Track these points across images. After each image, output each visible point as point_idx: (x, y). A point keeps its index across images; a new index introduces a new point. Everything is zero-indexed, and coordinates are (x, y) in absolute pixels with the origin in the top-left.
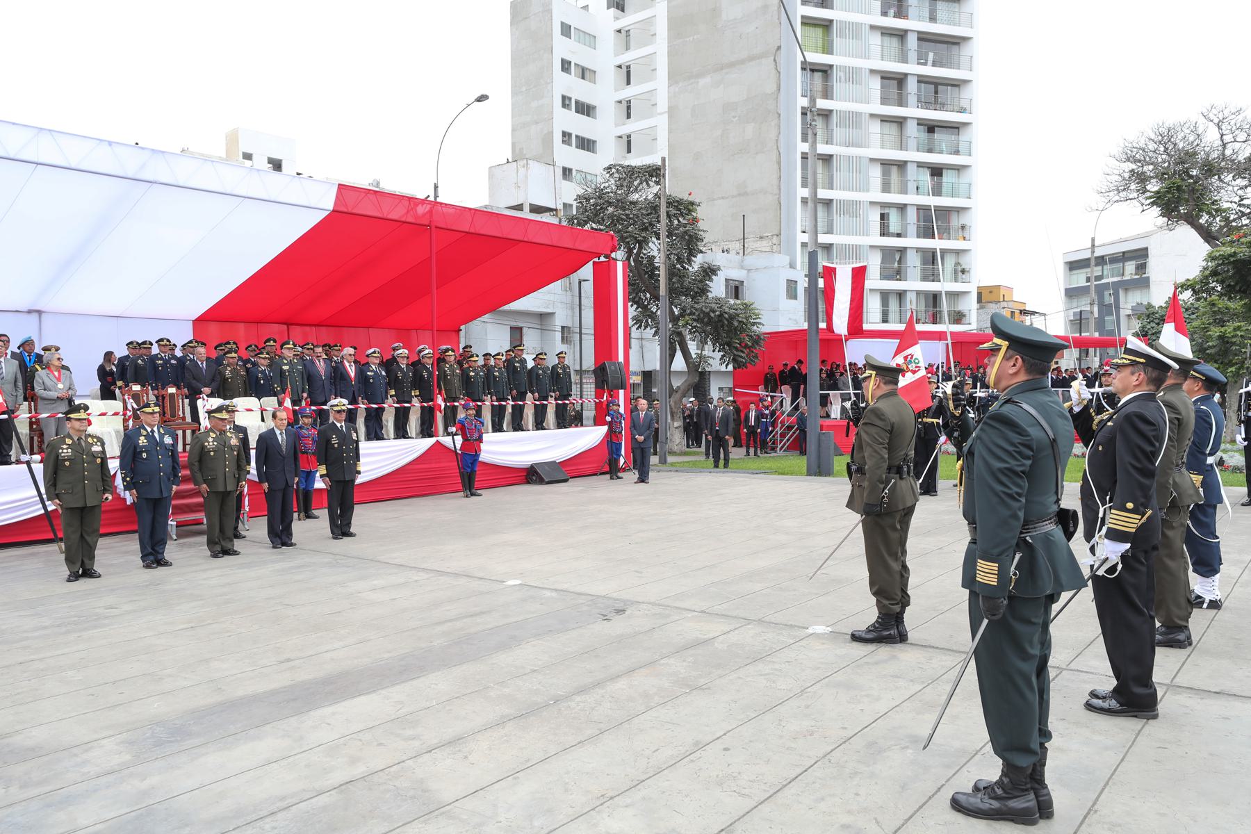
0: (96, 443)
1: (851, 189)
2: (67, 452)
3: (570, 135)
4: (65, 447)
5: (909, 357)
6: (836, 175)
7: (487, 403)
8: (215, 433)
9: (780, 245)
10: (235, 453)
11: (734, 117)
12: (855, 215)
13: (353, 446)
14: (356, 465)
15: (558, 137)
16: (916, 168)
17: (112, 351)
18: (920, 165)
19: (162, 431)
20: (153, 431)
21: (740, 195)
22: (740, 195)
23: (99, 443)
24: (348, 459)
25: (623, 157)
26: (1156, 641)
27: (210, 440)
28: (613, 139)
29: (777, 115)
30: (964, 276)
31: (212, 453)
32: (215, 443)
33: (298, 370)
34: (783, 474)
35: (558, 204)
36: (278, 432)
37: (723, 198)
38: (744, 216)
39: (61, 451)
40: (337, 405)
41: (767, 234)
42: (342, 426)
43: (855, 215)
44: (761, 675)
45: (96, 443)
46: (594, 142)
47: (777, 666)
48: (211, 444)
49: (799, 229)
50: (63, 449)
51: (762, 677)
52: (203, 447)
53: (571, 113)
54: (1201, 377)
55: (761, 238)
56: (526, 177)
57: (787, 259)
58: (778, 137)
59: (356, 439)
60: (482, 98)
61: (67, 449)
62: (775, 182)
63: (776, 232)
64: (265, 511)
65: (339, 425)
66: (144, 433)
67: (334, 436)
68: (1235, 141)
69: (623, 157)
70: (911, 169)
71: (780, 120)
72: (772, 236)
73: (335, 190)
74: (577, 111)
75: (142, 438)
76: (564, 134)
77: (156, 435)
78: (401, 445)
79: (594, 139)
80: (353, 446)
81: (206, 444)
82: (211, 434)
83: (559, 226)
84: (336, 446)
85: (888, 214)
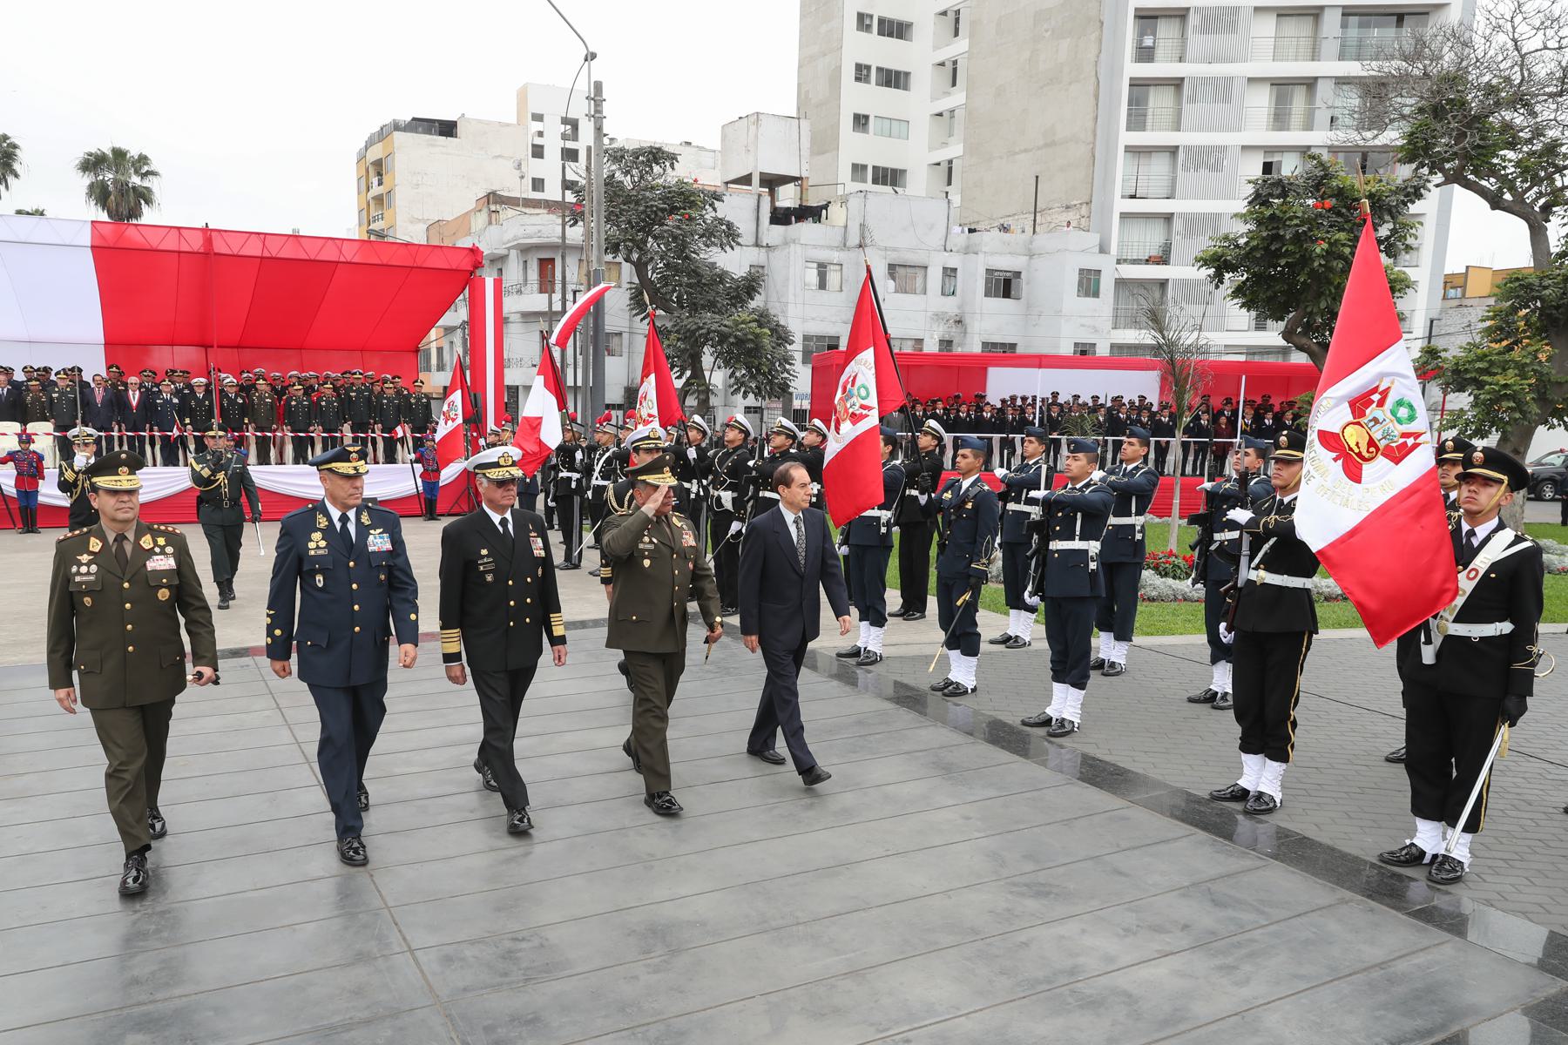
0: (162, 548)
1: (1211, 129)
2: (88, 573)
3: (868, 68)
4: (85, 558)
5: (1376, 397)
6: (1187, 108)
9: (1089, 217)
11: (1047, 31)
12: (1216, 167)
13: (534, 577)
15: (849, 72)
16: (1333, 86)
18: (1341, 81)
19: (365, 519)
20: (344, 519)
21: (1046, 145)
22: (1046, 145)
23: (169, 550)
25: (944, 93)
28: (930, 67)
29: (1099, 24)
30: (1407, 257)
34: (901, 657)
35: (803, 169)
37: (1026, 151)
38: (1037, 177)
39: (74, 569)
40: (496, 465)
41: (1075, 202)
42: (504, 522)
43: (1216, 167)
45: (162, 548)
46: (907, 74)
49: (1118, 193)
50: (80, 564)
53: (874, 37)
55: (1068, 207)
56: (756, 136)
57: (1093, 239)
58: (1098, 57)
59: (543, 553)
61: (88, 564)
62: (1090, 124)
63: (1086, 199)
65: (496, 518)
66: (322, 522)
67: (484, 552)
68: (1546, 48)
69: (944, 93)
70: (1324, 91)
71: (1102, 31)
72: (1081, 204)
73: (89, 227)
74: (881, 33)
75: (317, 536)
76: (859, 67)
77: (352, 528)
79: (907, 70)
84: (489, 578)
85: (1280, 163)
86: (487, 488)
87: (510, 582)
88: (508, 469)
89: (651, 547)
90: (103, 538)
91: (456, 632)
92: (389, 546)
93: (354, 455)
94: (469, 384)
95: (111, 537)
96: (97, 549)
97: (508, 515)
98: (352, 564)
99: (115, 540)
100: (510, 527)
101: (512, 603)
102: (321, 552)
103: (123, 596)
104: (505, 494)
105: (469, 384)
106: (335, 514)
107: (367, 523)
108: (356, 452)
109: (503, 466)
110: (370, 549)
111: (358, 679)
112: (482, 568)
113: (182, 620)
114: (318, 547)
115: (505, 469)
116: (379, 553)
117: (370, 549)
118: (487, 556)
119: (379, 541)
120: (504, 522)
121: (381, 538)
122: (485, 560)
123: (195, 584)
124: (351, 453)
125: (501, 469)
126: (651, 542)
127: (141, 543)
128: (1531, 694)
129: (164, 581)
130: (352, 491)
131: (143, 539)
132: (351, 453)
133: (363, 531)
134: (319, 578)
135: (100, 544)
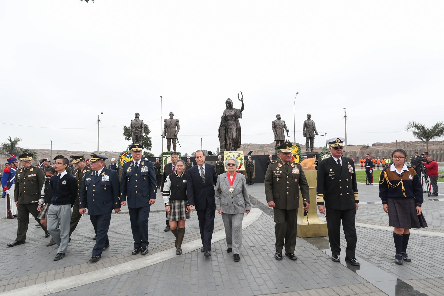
7: (407, 149)
13: (349, 179)
14: (353, 195)
17: (186, 153)
19: (142, 164)
20: (137, 163)
24: (344, 190)
26: (69, 161)
31: (278, 179)
32: (281, 172)
42: (339, 161)
48: (278, 172)
52: (273, 174)
54: (101, 159)
59: (353, 172)
64: (362, 205)
65: (336, 160)
66: (132, 164)
67: (331, 170)
75: (130, 168)
77: (138, 166)
78: (376, 184)
80: (349, 179)
81: (274, 172)
82: (279, 164)
83: (149, 203)
84: (333, 178)
86: (332, 150)
87: (340, 180)
88: (338, 144)
89: (278, 174)
90: (282, 163)
91: (322, 195)
92: (148, 171)
93: (137, 146)
95: (284, 164)
96: (281, 166)
97: (340, 159)
98: (136, 175)
99: (285, 165)
100: (341, 163)
101: (341, 187)
102: (129, 172)
103: (287, 180)
104: (338, 152)
106: (135, 162)
107: (143, 164)
108: (137, 146)
110: (141, 171)
111: (289, 208)
112: (330, 175)
113: (299, 187)
114: (129, 171)
115: (338, 144)
117: (141, 171)
118: (332, 171)
119: (145, 169)
120: (339, 161)
121: (145, 168)
122: (331, 172)
126: (279, 172)
127: (291, 165)
128: (396, 285)
130: (136, 155)
131: (291, 164)
133: (141, 166)
134: (128, 179)
135: (282, 165)
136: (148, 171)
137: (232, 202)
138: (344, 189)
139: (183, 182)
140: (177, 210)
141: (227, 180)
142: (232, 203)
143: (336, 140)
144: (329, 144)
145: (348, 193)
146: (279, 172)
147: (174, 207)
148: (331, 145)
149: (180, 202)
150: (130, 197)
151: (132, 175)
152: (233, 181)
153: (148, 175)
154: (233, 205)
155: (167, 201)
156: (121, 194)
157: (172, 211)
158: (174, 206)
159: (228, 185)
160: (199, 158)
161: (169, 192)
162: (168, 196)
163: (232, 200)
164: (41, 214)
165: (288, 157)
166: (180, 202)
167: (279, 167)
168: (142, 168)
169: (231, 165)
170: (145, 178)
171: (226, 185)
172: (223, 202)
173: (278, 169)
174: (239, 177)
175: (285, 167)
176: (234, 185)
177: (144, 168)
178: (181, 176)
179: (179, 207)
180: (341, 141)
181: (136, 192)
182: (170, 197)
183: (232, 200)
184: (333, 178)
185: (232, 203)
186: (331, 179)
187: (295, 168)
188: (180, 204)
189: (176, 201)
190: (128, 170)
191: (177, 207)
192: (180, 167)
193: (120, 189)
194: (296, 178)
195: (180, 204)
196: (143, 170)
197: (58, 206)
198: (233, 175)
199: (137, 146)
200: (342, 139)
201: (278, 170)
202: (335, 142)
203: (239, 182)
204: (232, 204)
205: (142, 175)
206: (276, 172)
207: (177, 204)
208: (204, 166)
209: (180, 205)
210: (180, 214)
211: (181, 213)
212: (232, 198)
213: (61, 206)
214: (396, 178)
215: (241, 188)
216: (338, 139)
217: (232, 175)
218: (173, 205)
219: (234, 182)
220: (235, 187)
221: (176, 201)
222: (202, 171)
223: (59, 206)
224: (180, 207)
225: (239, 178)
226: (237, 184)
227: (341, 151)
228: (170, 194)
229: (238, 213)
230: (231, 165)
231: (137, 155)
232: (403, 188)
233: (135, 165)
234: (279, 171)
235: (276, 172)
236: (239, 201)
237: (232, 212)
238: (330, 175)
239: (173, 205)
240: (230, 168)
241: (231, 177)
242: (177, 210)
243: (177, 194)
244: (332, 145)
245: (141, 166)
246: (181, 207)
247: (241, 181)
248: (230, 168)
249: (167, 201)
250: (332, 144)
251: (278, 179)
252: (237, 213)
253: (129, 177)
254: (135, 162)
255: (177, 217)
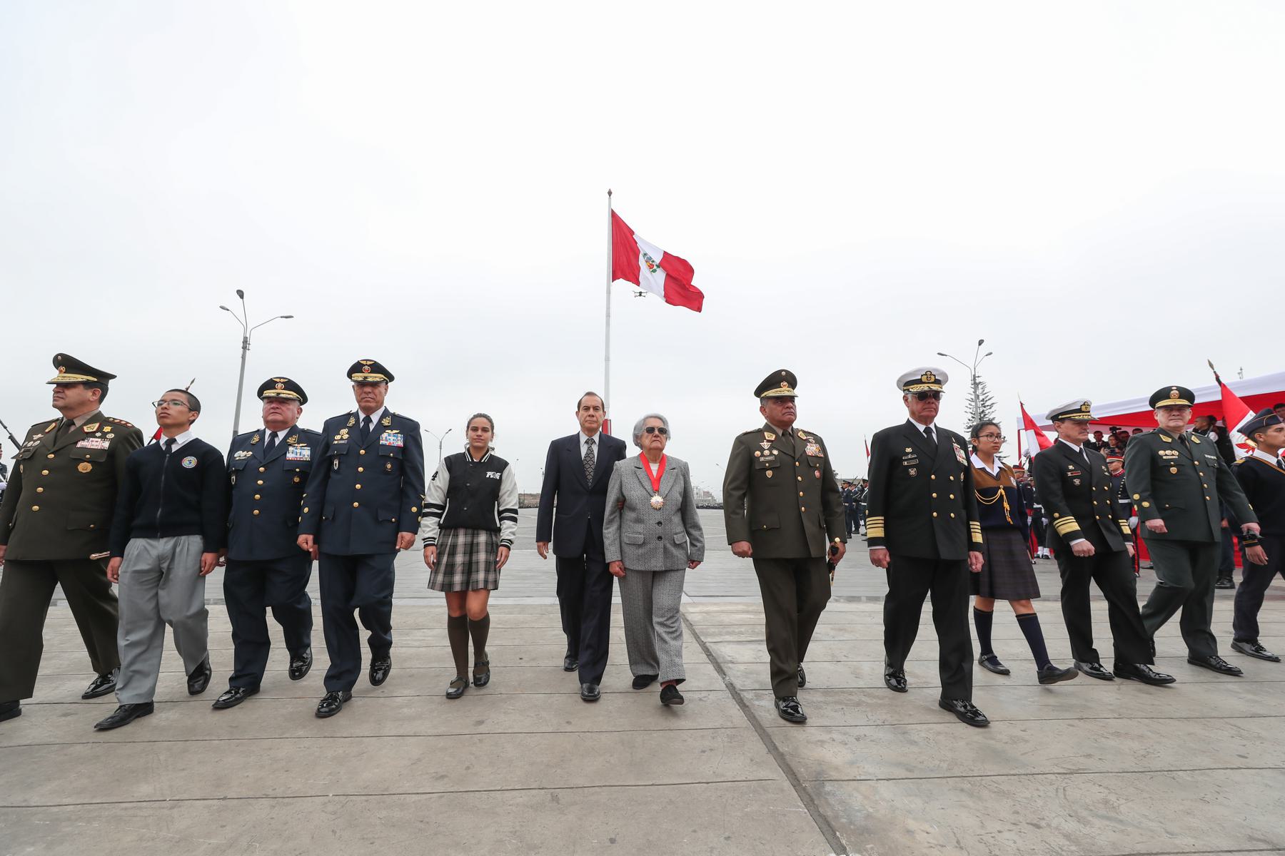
8: (774, 432)
10: (817, 474)
19: (386, 422)
27: (766, 445)
31: (769, 474)
32: (775, 452)
33: (1205, 463)
36: (583, 438)
44: (1121, 822)
47: (1071, 826)
48: (767, 452)
51: (1121, 817)
60: (610, 193)
65: (921, 428)
66: (352, 421)
67: (909, 450)
75: (344, 432)
77: (372, 427)
80: (957, 478)
81: (758, 453)
91: (880, 519)
92: (400, 443)
93: (366, 367)
94: (96, 380)
95: (780, 432)
104: (784, 411)
105: (96, 380)
106: (362, 416)
107: (387, 424)
108: (369, 366)
109: (925, 383)
110: (381, 442)
114: (342, 439)
116: (390, 448)
117: (381, 442)
119: (392, 438)
120: (928, 430)
121: (394, 436)
122: (909, 456)
123: (421, 468)
124: (365, 365)
125: (924, 385)
126: (771, 454)
129: (88, 456)
132: (365, 365)
134: (336, 462)
136: (400, 443)
137: (657, 536)
138: (943, 504)
139: (488, 476)
140: (459, 559)
141: (642, 474)
142: (660, 538)
143: (922, 376)
144: (905, 388)
145: (952, 515)
146: (771, 454)
147: (452, 547)
148: (908, 390)
149: (473, 534)
150: (333, 519)
151: (347, 454)
152: (660, 478)
153: (400, 457)
154: (661, 544)
155: (429, 531)
156: (306, 510)
157: (445, 559)
158: (454, 547)
159: (646, 487)
160: (591, 409)
161: (442, 508)
162: (437, 519)
163: (659, 528)
164: (487, 552)
165: (788, 410)
166: (473, 534)
167: (768, 441)
168: (384, 435)
169: (656, 432)
170: (389, 466)
171: (642, 488)
172: (629, 538)
173: (766, 445)
174: (673, 466)
175: (784, 440)
176: (664, 486)
177: (389, 435)
178: (483, 461)
179: (469, 549)
180: (935, 379)
181: (356, 504)
182: (441, 522)
183: (659, 530)
184: (913, 472)
185: (660, 538)
186: (908, 473)
187: (809, 442)
188: (472, 541)
189: (461, 532)
190: (338, 437)
191: (460, 549)
192: (479, 432)
193: (304, 495)
194: (817, 469)
195: (472, 541)
196: (386, 441)
197: (165, 540)
198: (658, 461)
199: (366, 367)
200: (938, 375)
201: (766, 447)
202: (919, 382)
203: (675, 481)
204: (658, 542)
205: (380, 454)
206: (762, 453)
207: (461, 539)
208: (596, 438)
209: (472, 544)
210: (466, 571)
211: (469, 568)
212: (659, 523)
213: (176, 538)
214: (992, 483)
215: (681, 496)
216: (929, 374)
217: (655, 461)
218: (449, 544)
219: (662, 479)
220: (666, 492)
221: (461, 532)
222: (590, 449)
223: (166, 542)
224: (471, 549)
225: (674, 469)
226: (670, 484)
227: (933, 405)
228: (443, 513)
229: (673, 569)
230: (656, 432)
231: (365, 393)
232: (1006, 505)
233: (362, 425)
234: (770, 449)
235: (762, 455)
236: (676, 534)
237: (657, 564)
238: (906, 463)
239: (449, 544)
240: (654, 439)
241: (654, 468)
242: (459, 559)
243: (465, 509)
244: (910, 390)
245: (381, 428)
246: (475, 548)
247: (681, 477)
248: (654, 439)
249: (429, 531)
250: (912, 387)
251: (769, 474)
252: (671, 568)
253: (339, 456)
254: (362, 416)
255: (458, 578)
